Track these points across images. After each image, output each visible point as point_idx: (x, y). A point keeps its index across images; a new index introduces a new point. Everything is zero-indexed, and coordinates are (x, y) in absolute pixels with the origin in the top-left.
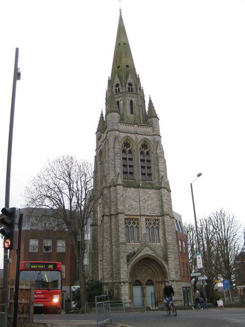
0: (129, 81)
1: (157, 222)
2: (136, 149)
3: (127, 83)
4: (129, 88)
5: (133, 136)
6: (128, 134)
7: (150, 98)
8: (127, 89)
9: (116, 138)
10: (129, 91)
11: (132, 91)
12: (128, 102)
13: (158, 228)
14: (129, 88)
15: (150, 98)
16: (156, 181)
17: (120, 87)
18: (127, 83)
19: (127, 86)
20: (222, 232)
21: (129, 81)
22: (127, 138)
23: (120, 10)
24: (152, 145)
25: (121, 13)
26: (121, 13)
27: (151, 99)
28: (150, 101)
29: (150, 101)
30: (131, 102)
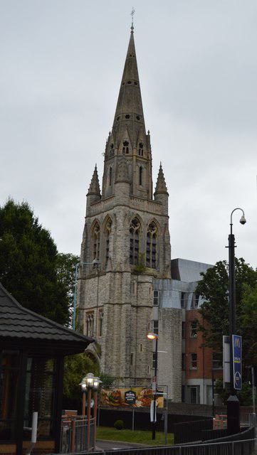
11: (127, 152)
14: (124, 148)
23: (132, 28)
25: (132, 32)
26: (132, 32)
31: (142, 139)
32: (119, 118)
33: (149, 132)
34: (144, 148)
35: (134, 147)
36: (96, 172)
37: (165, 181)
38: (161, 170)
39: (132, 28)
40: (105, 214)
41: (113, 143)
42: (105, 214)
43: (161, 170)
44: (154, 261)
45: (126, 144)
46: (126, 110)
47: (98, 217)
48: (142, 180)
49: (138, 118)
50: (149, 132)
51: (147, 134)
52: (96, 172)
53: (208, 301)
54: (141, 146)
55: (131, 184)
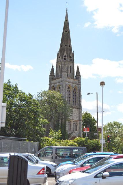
0: (70, 56)
1: (77, 123)
2: (72, 90)
3: (64, 56)
4: (64, 58)
5: (71, 84)
6: (70, 83)
7: (53, 65)
8: (63, 59)
9: (66, 85)
10: (64, 60)
11: (66, 60)
12: (70, 66)
13: (77, 125)
14: (64, 58)
15: (53, 65)
16: (78, 105)
17: (67, 58)
18: (64, 56)
19: (64, 57)
20: (62, 120)
21: (70, 56)
22: (75, 86)
23: (67, 9)
24: (77, 89)
25: (67, 11)
26: (67, 11)
27: (79, 66)
28: (78, 68)
29: (78, 68)
30: (71, 66)
31: (71, 55)
32: (62, 46)
33: (73, 51)
34: (72, 58)
35: (69, 58)
36: (53, 67)
37: (80, 73)
38: (78, 67)
39: (67, 9)
40: (58, 84)
41: (60, 56)
42: (58, 84)
43: (78, 67)
44: (75, 123)
45: (65, 56)
46: (63, 38)
47: (55, 85)
48: (71, 71)
49: (68, 32)
50: (73, 51)
51: (73, 52)
52: (53, 67)
53: (13, 110)
54: (71, 57)
55: (68, 73)
